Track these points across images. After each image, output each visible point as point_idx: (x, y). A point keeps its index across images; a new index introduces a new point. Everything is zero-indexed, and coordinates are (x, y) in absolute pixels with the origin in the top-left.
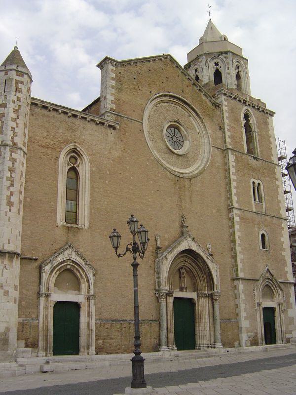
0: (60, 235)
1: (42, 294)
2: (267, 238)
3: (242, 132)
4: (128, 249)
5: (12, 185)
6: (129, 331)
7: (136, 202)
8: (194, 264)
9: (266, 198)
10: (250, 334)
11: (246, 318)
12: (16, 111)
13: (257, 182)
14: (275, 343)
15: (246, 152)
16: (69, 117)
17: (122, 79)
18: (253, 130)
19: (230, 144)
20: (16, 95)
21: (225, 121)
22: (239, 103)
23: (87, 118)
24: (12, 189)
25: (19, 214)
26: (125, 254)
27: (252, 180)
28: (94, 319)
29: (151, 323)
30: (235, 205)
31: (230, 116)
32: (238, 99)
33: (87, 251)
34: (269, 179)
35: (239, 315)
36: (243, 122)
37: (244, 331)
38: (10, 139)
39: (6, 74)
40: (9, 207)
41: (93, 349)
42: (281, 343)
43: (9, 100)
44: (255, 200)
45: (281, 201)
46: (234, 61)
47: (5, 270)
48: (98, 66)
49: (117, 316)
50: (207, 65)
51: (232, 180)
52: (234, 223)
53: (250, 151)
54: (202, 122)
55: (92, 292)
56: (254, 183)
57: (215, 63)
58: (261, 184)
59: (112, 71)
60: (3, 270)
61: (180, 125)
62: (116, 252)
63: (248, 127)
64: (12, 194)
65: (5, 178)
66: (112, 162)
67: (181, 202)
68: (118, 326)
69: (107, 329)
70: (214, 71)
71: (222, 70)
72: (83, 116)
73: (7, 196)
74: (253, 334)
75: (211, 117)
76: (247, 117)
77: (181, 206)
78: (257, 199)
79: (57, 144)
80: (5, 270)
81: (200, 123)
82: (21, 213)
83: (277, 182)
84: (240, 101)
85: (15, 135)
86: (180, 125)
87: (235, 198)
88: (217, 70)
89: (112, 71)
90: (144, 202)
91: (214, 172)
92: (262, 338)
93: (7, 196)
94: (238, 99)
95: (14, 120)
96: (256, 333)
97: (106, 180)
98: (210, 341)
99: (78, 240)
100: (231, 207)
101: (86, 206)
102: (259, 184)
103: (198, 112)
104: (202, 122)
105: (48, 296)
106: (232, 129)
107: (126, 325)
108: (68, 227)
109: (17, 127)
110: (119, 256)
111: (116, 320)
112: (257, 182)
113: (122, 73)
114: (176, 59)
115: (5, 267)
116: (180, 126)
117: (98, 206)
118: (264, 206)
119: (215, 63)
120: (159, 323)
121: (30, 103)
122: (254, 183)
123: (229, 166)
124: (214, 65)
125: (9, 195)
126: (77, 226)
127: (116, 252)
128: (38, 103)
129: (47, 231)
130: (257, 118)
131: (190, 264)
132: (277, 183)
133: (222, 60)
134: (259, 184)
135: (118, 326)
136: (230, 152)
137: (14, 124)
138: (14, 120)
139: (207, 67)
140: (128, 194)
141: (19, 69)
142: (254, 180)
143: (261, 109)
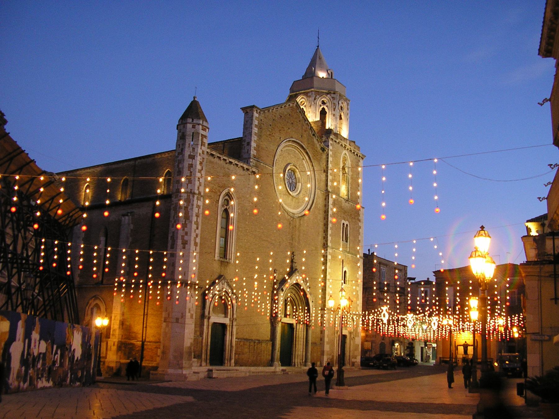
1: (206, 316)
3: (339, 176)
6: (254, 348)
8: (296, 295)
9: (351, 238)
10: (329, 356)
11: (328, 343)
17: (262, 125)
20: (201, 149)
21: (329, 165)
22: (341, 147)
23: (238, 165)
27: (343, 221)
28: (235, 338)
29: (267, 343)
31: (333, 160)
32: (340, 144)
34: (354, 220)
35: (323, 340)
37: (325, 353)
39: (193, 127)
40: (195, 247)
41: (233, 361)
42: (349, 365)
43: (197, 153)
44: (343, 240)
45: (361, 241)
47: (191, 298)
49: (247, 336)
50: (315, 101)
52: (327, 260)
54: (313, 166)
55: (235, 316)
56: (343, 224)
58: (349, 225)
61: (297, 168)
65: (193, 223)
66: (251, 204)
67: (293, 241)
68: (248, 344)
69: (241, 346)
72: (236, 163)
73: (195, 238)
74: (331, 357)
75: (319, 161)
77: (292, 244)
79: (218, 188)
80: (191, 298)
81: (311, 166)
84: (342, 145)
86: (297, 168)
90: (269, 240)
91: (317, 213)
92: (303, 355)
93: (195, 238)
94: (340, 144)
96: (333, 356)
97: (246, 221)
98: (302, 360)
99: (227, 272)
101: (233, 243)
102: (347, 225)
103: (311, 156)
104: (313, 166)
105: (209, 318)
107: (252, 344)
111: (247, 340)
113: (262, 120)
115: (192, 295)
116: (296, 169)
117: (241, 244)
118: (348, 245)
122: (343, 224)
123: (328, 208)
125: (195, 237)
126: (226, 261)
128: (214, 154)
129: (209, 265)
130: (352, 161)
131: (294, 295)
132: (360, 224)
134: (347, 225)
135: (248, 344)
138: (200, 171)
139: (315, 104)
140: (259, 233)
141: (204, 124)
143: (355, 154)
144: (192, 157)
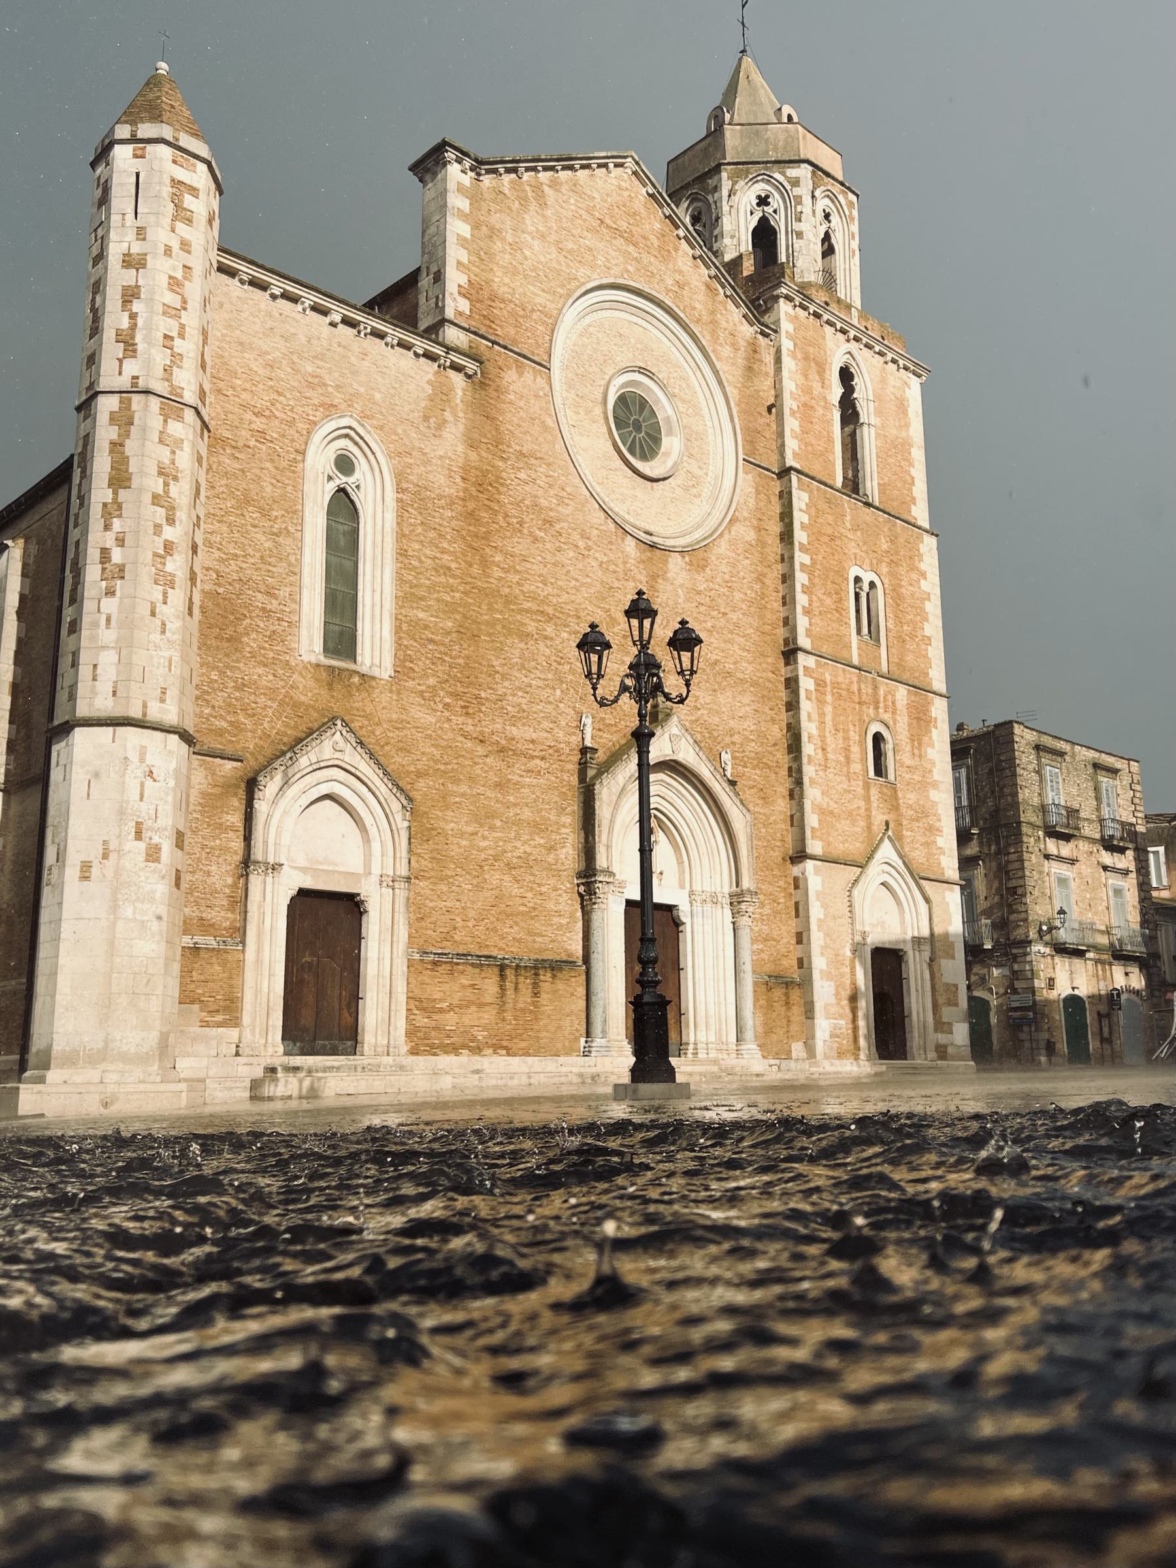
0: (307, 690)
2: (888, 747)
4: (624, 688)
5: (171, 521)
7: (527, 611)
12: (175, 284)
13: (868, 577)
14: (906, 1059)
15: (839, 482)
16: (333, 325)
18: (863, 418)
19: (795, 454)
24: (169, 533)
25: (190, 614)
26: (616, 700)
30: (803, 641)
33: (387, 744)
36: (837, 391)
38: (160, 372)
44: (859, 632)
46: (817, 193)
47: (149, 782)
48: (414, 168)
51: (797, 566)
53: (853, 486)
56: (858, 580)
57: (759, 197)
59: (460, 189)
60: (142, 785)
62: (594, 689)
63: (849, 412)
64: (169, 547)
70: (754, 222)
71: (780, 223)
76: (846, 375)
78: (865, 630)
82: (196, 611)
83: (922, 582)
85: (177, 358)
87: (802, 622)
88: (764, 221)
89: (460, 189)
95: (171, 312)
100: (792, 646)
102: (872, 585)
106: (806, 411)
108: (331, 669)
109: (182, 336)
110: (602, 703)
112: (868, 577)
114: (428, 149)
119: (759, 197)
120: (378, 1158)
121: (215, 265)
122: (858, 580)
124: (754, 202)
127: (594, 689)
133: (780, 187)
134: (872, 585)
136: (794, 477)
137: (169, 326)
138: (171, 312)
142: (861, 573)
144: (132, 262)
